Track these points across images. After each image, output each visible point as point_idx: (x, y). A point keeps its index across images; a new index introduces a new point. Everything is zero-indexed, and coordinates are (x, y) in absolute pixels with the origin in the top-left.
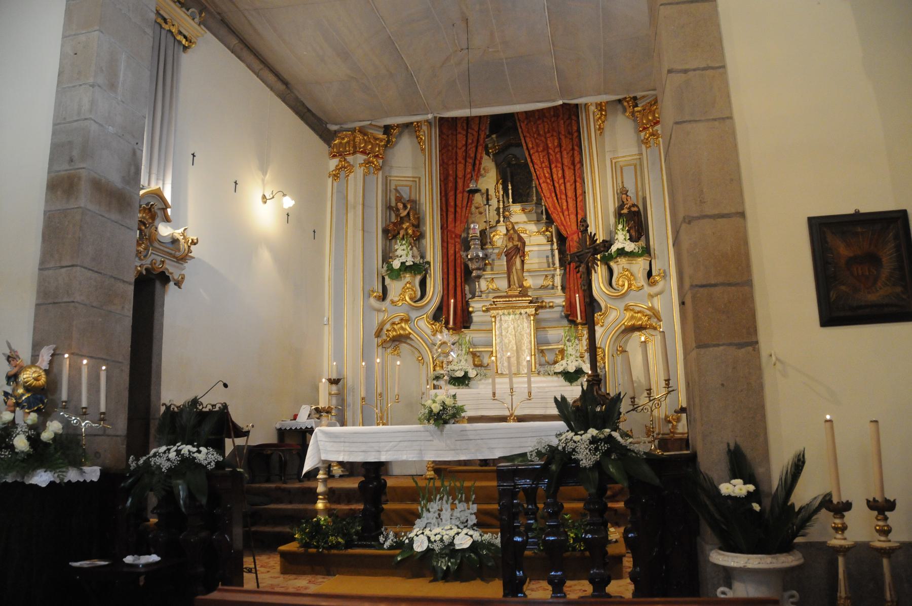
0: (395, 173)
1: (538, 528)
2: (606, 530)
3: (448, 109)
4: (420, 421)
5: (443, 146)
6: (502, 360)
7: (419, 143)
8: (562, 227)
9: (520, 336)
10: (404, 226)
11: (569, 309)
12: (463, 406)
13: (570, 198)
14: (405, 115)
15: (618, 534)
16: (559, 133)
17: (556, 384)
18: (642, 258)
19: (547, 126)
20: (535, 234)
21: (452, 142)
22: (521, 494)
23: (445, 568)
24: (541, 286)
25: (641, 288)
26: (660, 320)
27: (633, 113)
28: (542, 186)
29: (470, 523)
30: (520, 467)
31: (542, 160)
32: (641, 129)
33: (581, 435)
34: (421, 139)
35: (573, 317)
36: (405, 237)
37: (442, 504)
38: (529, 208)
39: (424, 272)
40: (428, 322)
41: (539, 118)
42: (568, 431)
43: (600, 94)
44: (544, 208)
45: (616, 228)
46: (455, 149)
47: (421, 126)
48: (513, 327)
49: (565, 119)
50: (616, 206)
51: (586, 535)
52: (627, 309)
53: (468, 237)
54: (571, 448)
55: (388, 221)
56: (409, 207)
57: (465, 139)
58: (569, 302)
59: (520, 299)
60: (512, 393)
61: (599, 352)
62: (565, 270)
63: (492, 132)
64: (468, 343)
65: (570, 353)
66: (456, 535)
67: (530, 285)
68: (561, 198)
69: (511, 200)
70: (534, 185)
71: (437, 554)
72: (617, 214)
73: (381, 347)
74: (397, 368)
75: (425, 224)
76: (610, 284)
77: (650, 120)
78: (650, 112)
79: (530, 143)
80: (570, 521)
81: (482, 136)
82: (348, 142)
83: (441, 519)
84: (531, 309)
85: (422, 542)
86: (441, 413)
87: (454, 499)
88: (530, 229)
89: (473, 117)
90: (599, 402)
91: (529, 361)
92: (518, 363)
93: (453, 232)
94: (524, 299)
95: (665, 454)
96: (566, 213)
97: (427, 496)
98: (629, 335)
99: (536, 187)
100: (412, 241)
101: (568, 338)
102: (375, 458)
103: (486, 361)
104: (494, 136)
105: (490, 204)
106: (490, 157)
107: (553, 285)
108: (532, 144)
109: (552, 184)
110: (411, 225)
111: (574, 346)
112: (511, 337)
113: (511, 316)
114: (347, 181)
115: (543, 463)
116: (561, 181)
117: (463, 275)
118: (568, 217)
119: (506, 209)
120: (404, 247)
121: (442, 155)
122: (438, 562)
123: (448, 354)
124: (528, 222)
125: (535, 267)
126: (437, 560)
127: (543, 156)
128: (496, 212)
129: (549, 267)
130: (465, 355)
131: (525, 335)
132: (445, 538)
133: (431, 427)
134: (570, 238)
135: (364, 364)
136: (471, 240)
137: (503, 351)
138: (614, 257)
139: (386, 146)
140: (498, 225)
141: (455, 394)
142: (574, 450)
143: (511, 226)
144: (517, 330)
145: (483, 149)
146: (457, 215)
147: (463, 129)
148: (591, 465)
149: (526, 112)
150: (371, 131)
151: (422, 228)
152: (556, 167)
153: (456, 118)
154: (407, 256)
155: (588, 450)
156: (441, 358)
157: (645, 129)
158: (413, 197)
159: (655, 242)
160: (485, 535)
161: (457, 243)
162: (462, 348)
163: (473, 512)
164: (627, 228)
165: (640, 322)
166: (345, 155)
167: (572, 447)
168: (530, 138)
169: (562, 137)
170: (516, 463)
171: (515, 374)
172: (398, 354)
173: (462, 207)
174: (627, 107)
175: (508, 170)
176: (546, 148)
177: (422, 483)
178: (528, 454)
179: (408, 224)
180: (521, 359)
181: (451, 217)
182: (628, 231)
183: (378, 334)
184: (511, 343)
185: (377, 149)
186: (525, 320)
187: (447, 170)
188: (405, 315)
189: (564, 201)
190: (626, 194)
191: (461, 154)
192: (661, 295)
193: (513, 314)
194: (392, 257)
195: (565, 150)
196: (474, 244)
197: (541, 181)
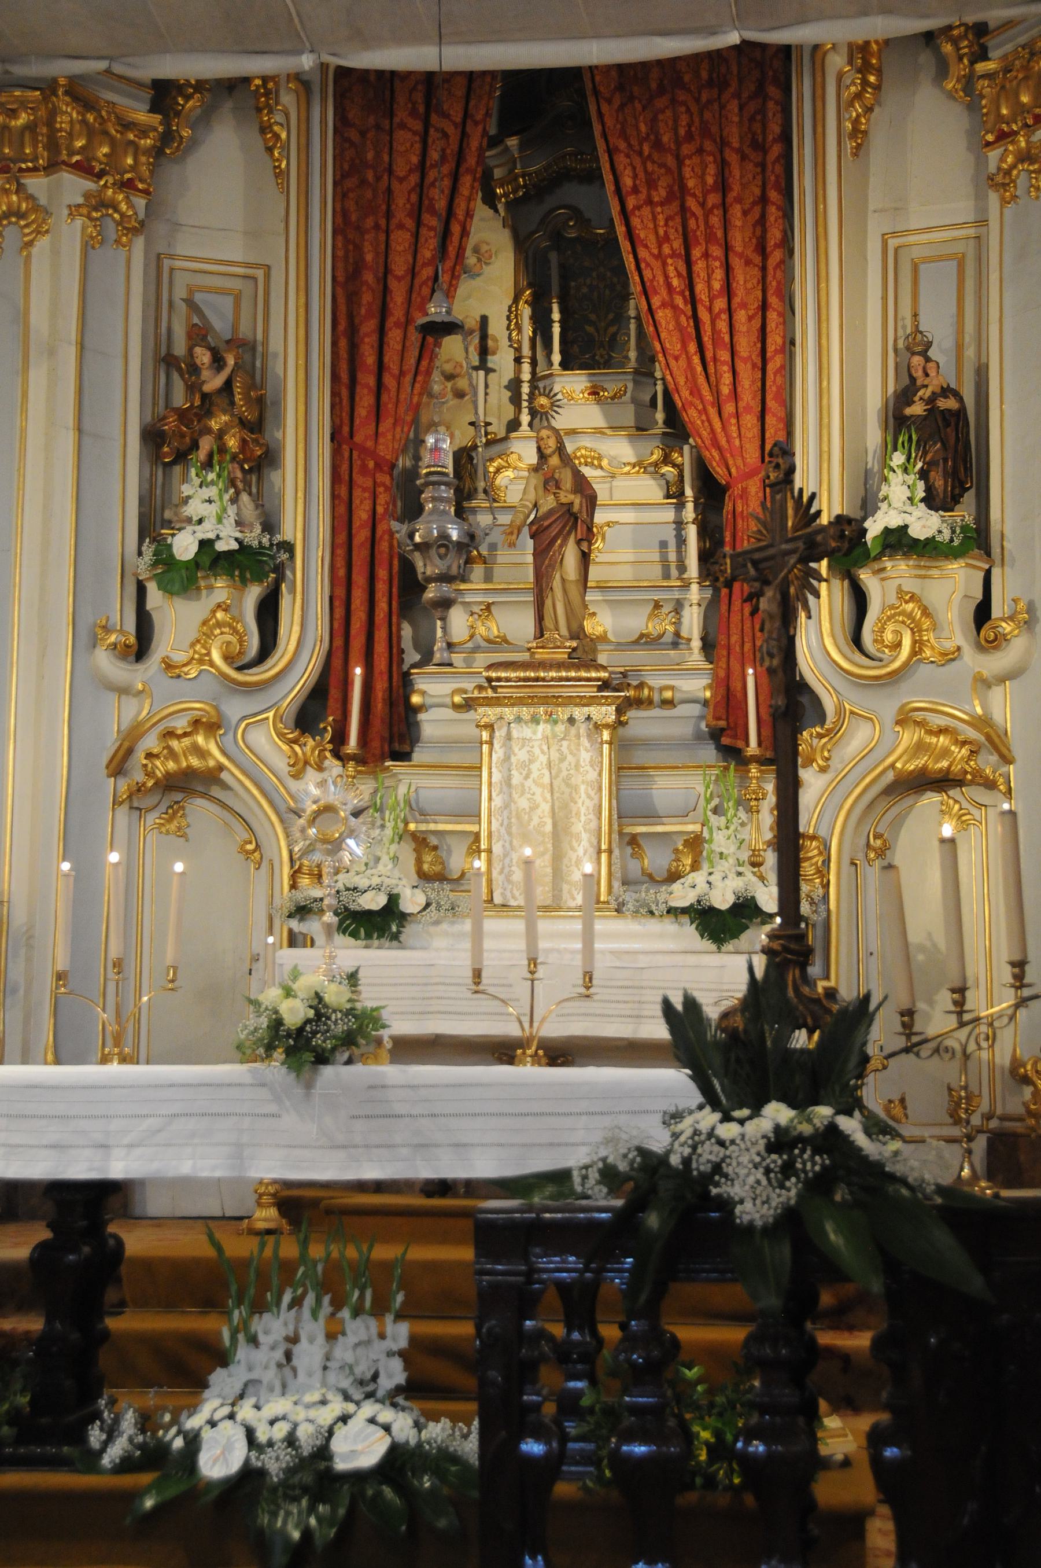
0: (186, 246)
1: (597, 1407)
2: (813, 1418)
3: (364, 40)
4: (243, 1053)
5: (346, 167)
6: (507, 861)
7: (270, 150)
8: (715, 454)
9: (567, 790)
10: (214, 424)
11: (722, 712)
12: (377, 1009)
13: (745, 360)
14: (223, 52)
15: (850, 1437)
16: (723, 143)
17: (671, 946)
18: (962, 562)
19: (684, 120)
20: (627, 469)
21: (378, 155)
22: (552, 1297)
23: (296, 1535)
24: (637, 636)
25: (951, 657)
26: (1007, 760)
27: (969, 82)
28: (657, 317)
29: (386, 1384)
30: (547, 1215)
31: (661, 232)
32: (990, 138)
33: (742, 1122)
34: (277, 136)
35: (735, 737)
36: (216, 458)
37: (298, 1320)
38: (612, 387)
39: (273, 575)
40: (281, 735)
41: (661, 91)
42: (701, 1107)
43: (865, 14)
44: (659, 388)
45: (884, 463)
46: (386, 177)
47: (277, 92)
48: (545, 762)
49: (745, 95)
50: (891, 390)
51: (747, 1442)
52: (904, 719)
53: (416, 468)
54: (709, 1161)
55: (162, 402)
56: (231, 361)
57: (418, 146)
58: (722, 691)
59: (573, 674)
60: (532, 973)
61: (811, 849)
62: (716, 590)
63: (506, 129)
64: (402, 805)
65: (719, 850)
66: (340, 1424)
67: (605, 632)
68: (715, 359)
69: (556, 358)
70: (632, 313)
71: (274, 1489)
72: (891, 421)
73: (125, 807)
74: (175, 881)
75: (279, 421)
76: (857, 641)
77: (1024, 105)
78: (1026, 78)
79: (628, 172)
80: (699, 1388)
81: (474, 143)
82: (31, 128)
83: (294, 1370)
84: (604, 708)
85: (228, 1448)
86: (308, 1028)
87: (338, 1304)
88: (612, 453)
89: (446, 73)
90: (801, 1021)
91: (591, 875)
92: (558, 874)
93: (373, 454)
94: (584, 674)
95: (1005, 1193)
96: (729, 408)
97: (252, 1291)
98: (908, 801)
99: (638, 318)
100: (239, 474)
101: (716, 802)
102: (91, 1170)
103: (457, 862)
104: (513, 142)
105: (490, 365)
106: (496, 211)
107: (677, 634)
108: (635, 177)
109: (690, 313)
110: (237, 421)
111: (732, 828)
112: (538, 791)
113: (541, 727)
114: (28, 259)
115: (619, 1203)
116: (720, 304)
117: (395, 590)
118: (733, 421)
119: (541, 385)
120: (213, 492)
121: (344, 195)
122: (274, 1515)
123: (336, 846)
124: (608, 431)
125: (624, 574)
126: (272, 1507)
127: (667, 220)
128: (509, 394)
129: (667, 576)
130: (392, 841)
131: (583, 788)
132: (305, 1432)
133: (275, 1069)
134: (737, 490)
135: (66, 866)
136: (427, 484)
137: (510, 834)
138: (873, 555)
139: (158, 152)
140: (513, 435)
141: (357, 972)
142: (717, 1168)
143: (552, 443)
144: (560, 771)
145: (476, 184)
146: (384, 398)
147: (413, 113)
148: (771, 1220)
149: (621, 68)
150: (110, 96)
151: (273, 434)
152: (706, 255)
153: (393, 73)
154: (220, 520)
155: (761, 1170)
156: (317, 857)
157: (1003, 137)
158: (244, 330)
159: (1008, 511)
160: (431, 1424)
161: (381, 489)
162: (383, 819)
163: (395, 1348)
164: (920, 465)
165: (944, 764)
166: (21, 170)
167: (713, 1158)
168: (628, 156)
169: (732, 158)
170: (536, 1200)
171: (546, 908)
172: (179, 829)
173: (402, 373)
174: (952, 60)
175: (553, 257)
176: (679, 192)
177: (238, 1247)
178: (575, 1173)
179: (225, 418)
180: (565, 861)
181: (365, 402)
182: (923, 475)
183: (118, 767)
184: (539, 811)
185: (130, 161)
186: (585, 741)
187: (358, 248)
188: (207, 708)
189: (725, 368)
190: (924, 354)
191: (401, 202)
192: (1015, 682)
193: (546, 721)
194: (170, 522)
195: (739, 200)
196: (434, 499)
197: (656, 301)
